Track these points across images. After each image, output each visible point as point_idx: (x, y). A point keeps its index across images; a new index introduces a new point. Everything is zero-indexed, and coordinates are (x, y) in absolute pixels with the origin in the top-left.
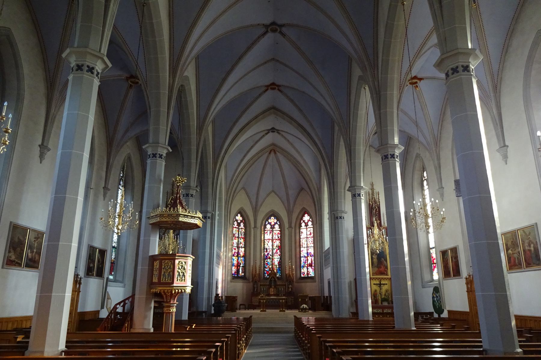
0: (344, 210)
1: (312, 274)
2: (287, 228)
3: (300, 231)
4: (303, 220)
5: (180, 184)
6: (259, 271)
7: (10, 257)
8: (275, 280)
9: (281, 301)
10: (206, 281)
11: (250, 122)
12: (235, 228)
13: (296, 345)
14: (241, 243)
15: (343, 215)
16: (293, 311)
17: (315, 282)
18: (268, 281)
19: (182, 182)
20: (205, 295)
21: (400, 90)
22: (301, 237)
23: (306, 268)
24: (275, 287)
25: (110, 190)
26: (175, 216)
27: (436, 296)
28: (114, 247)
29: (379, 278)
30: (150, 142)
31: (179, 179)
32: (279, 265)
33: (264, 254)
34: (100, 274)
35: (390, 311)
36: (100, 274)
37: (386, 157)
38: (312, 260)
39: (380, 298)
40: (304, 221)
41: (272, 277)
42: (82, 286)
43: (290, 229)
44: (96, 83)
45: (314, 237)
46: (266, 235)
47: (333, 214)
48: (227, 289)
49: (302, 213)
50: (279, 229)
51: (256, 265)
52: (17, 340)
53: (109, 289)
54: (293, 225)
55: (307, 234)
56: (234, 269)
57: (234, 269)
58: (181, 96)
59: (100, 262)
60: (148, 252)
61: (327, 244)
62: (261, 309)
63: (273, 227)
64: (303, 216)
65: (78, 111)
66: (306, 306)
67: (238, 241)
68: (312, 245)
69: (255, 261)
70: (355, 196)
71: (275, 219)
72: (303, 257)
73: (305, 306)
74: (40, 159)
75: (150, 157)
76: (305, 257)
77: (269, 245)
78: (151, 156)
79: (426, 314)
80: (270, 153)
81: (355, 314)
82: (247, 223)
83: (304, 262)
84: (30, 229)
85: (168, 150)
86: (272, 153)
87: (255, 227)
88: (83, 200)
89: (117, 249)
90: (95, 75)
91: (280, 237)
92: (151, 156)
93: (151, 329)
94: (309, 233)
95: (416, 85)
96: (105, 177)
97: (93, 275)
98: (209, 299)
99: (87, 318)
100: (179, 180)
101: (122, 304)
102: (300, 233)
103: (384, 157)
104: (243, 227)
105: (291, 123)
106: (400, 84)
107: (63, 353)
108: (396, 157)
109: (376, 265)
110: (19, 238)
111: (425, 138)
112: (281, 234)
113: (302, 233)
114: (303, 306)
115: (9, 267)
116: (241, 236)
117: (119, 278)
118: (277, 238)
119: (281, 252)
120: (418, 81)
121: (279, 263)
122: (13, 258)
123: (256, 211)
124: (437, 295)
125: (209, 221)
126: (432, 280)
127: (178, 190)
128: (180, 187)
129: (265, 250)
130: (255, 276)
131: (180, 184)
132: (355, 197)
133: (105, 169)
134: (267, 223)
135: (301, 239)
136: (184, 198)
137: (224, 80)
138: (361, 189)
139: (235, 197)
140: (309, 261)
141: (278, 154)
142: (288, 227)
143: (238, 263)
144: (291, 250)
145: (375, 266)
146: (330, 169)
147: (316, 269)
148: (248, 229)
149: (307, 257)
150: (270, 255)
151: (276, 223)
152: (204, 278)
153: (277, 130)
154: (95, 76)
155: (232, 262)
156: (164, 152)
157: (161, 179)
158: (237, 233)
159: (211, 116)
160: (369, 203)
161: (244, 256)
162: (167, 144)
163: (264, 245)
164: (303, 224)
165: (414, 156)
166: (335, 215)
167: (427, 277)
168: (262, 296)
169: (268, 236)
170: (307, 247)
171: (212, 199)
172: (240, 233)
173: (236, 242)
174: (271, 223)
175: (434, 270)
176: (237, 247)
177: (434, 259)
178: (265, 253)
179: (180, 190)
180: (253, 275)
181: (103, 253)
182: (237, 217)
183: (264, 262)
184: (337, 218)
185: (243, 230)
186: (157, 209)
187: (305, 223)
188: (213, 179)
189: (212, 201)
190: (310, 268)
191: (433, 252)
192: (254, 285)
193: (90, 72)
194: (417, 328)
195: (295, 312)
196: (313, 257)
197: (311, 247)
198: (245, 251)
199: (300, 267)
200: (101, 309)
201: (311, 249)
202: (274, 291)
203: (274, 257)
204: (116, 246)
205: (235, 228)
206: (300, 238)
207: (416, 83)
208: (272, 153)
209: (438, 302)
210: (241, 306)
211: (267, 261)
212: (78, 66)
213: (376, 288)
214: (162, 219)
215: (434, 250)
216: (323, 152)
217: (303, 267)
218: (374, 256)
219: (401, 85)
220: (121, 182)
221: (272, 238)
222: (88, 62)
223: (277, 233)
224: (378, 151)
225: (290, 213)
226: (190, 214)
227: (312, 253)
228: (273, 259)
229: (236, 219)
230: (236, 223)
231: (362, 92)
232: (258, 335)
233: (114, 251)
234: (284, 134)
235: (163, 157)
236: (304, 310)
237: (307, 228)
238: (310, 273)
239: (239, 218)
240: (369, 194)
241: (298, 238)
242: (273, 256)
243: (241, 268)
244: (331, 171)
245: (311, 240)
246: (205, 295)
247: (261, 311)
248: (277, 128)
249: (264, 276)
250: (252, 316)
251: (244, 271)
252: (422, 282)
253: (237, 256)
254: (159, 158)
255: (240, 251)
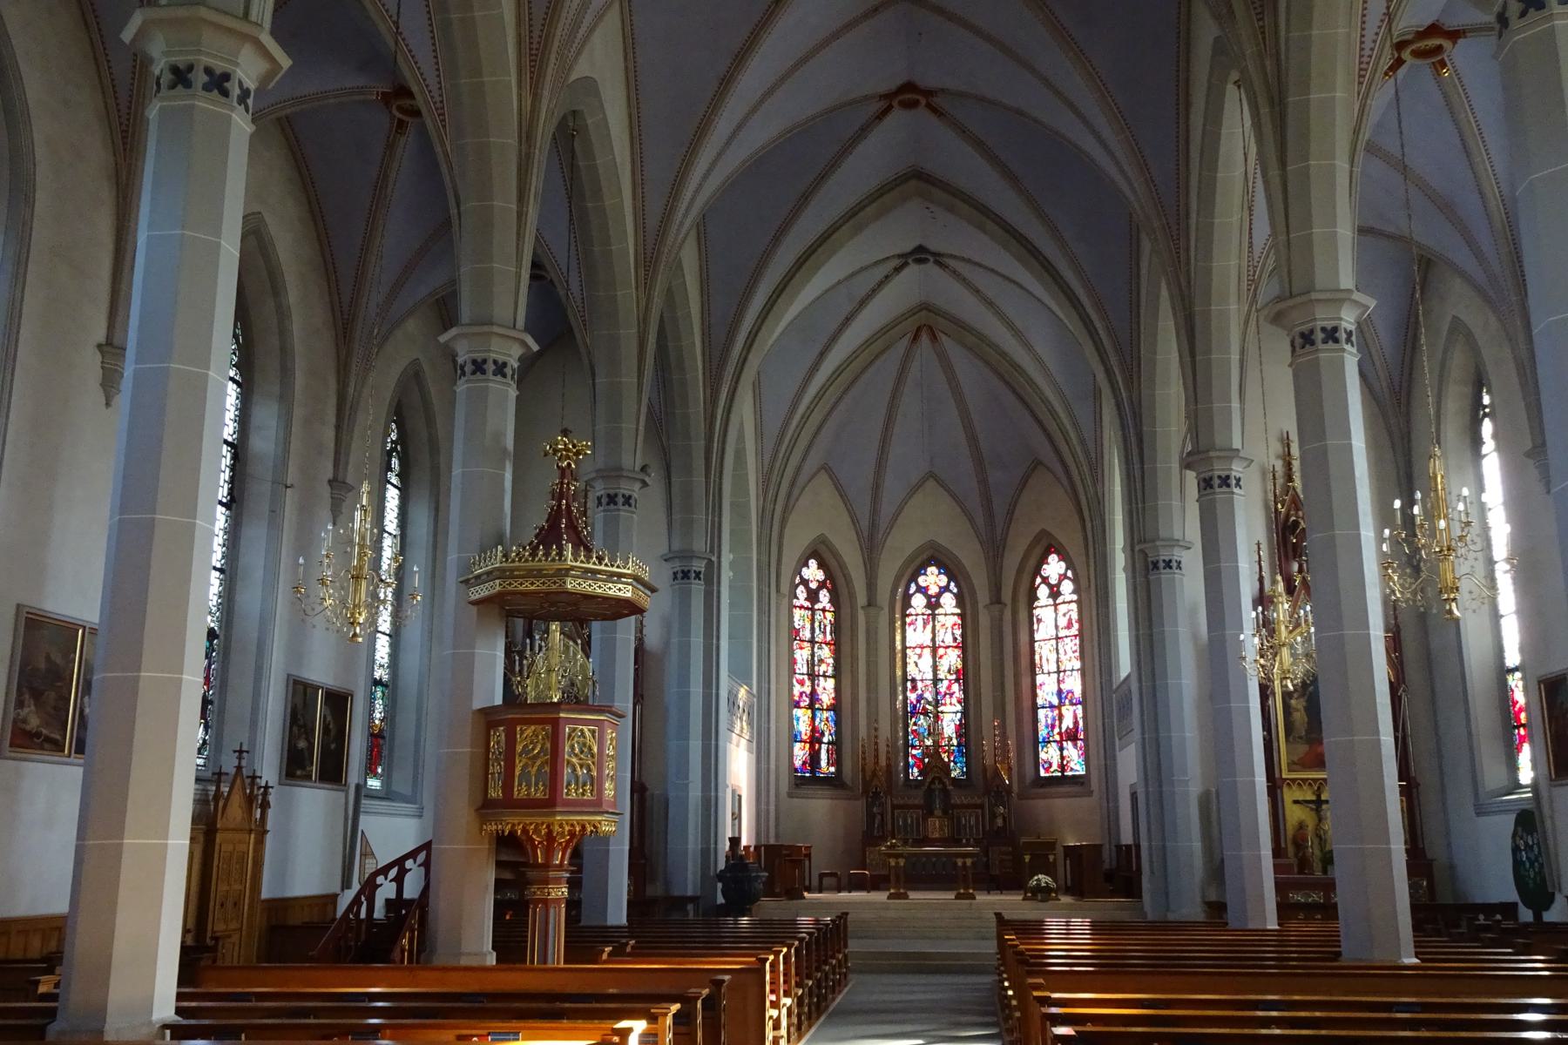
0: (1181, 538)
1: (1077, 766)
2: (986, 607)
3: (1031, 616)
4: (1042, 577)
5: (569, 464)
6: (888, 758)
7: (25, 721)
8: (945, 791)
9: (892, 862)
10: (695, 792)
11: (834, 232)
12: (801, 607)
13: (993, 1014)
14: (821, 661)
15: (1177, 554)
16: (1008, 898)
17: (1090, 793)
18: (921, 793)
19: (577, 453)
20: (693, 843)
21: (1360, 83)
22: (1037, 637)
23: (1054, 744)
24: (945, 812)
25: (353, 488)
26: (552, 576)
27: (1526, 844)
28: (378, 683)
29: (1315, 780)
30: (463, 322)
31: (565, 444)
32: (959, 736)
33: (905, 698)
34: (333, 773)
35: (1316, 897)
36: (333, 773)
37: (1307, 338)
38: (1075, 717)
39: (1317, 852)
40: (1047, 578)
41: (933, 779)
42: (271, 813)
43: (997, 607)
44: (241, 124)
45: (1081, 635)
46: (909, 630)
47: (1142, 551)
48: (777, 818)
49: (1038, 551)
50: (958, 611)
51: (876, 737)
52: (37, 989)
53: (365, 822)
54: (1007, 595)
55: (1057, 627)
56: (802, 753)
57: (800, 753)
58: (573, 151)
59: (333, 733)
60: (469, 697)
61: (1125, 665)
62: (889, 890)
63: (933, 604)
64: (1043, 560)
65: (183, 228)
66: (1049, 879)
67: (813, 655)
68: (1078, 665)
69: (873, 719)
70: (1214, 485)
71: (940, 573)
72: (1043, 707)
73: (1044, 879)
74: (105, 390)
75: (463, 374)
76: (1052, 707)
77: (920, 667)
78: (469, 368)
79: (1490, 909)
80: (916, 337)
81: (1217, 909)
82: (843, 591)
83: (1047, 726)
84: (84, 628)
85: (524, 344)
86: (925, 338)
87: (871, 603)
88: (1364, 446)
89: (390, 687)
90: (235, 99)
91: (959, 639)
92: (466, 369)
93: (489, 958)
94: (1063, 622)
95: (1439, 58)
96: (332, 445)
97: (308, 777)
98: (707, 853)
99: (296, 918)
100: (564, 450)
101: (393, 873)
102: (1031, 624)
103: (1299, 341)
104: (828, 606)
105: (981, 228)
106: (1361, 63)
107: (168, 1032)
108: (1344, 336)
109: (1304, 733)
110: (48, 658)
111: (1478, 254)
112: (963, 626)
113: (1039, 621)
114: (1038, 880)
115: (19, 755)
116: (821, 636)
117: (401, 784)
118: (949, 640)
119: (965, 691)
120: (1446, 44)
121: (958, 728)
122: (34, 722)
123: (871, 547)
124: (1531, 843)
125: (698, 588)
126: (1516, 786)
127: (562, 483)
128: (568, 472)
129: (909, 685)
130: (874, 774)
131: (569, 464)
132: (1211, 487)
133: (331, 418)
134: (913, 588)
135: (1036, 644)
136: (601, 508)
137: (726, 82)
138: (1230, 459)
139: (797, 500)
140: (1068, 723)
141: (944, 338)
142: (988, 601)
143: (814, 729)
144: (1003, 684)
145: (1301, 738)
146: (1129, 389)
147: (1093, 751)
148: (846, 611)
149: (1059, 707)
150: (929, 703)
151: (946, 589)
152: (687, 785)
153: (934, 254)
154: (235, 104)
155: (791, 726)
156: (512, 355)
157: (506, 449)
158: (808, 626)
159: (685, 216)
160: (1276, 509)
161: (835, 707)
162: (521, 322)
163: (905, 664)
164: (1043, 592)
165: (1445, 328)
166: (1146, 555)
167: (1493, 775)
168: (893, 846)
169: (917, 635)
170: (1058, 672)
171: (707, 509)
172: (817, 624)
173: (805, 658)
174: (927, 588)
175: (1519, 750)
176: (808, 674)
177: (1521, 710)
178: (908, 694)
179: (568, 484)
180: (869, 773)
181: (338, 701)
182: (804, 570)
183: (906, 725)
184: (1155, 565)
185: (829, 616)
186: (491, 552)
187: (1051, 587)
188: (709, 439)
189: (707, 515)
190: (1068, 745)
191: (1515, 682)
192: (869, 807)
193: (216, 91)
194: (1423, 960)
195: (1011, 903)
196: (1080, 707)
197: (1073, 670)
198: (837, 689)
199: (1036, 742)
200: (343, 890)
201: (1072, 678)
202: (941, 829)
203: (939, 709)
204: (385, 678)
205: (801, 607)
206: (1032, 641)
207: (1439, 49)
208: (925, 338)
209: (1532, 865)
210: (826, 881)
211: (915, 724)
212: (175, 70)
213: (1303, 817)
214: (510, 584)
215: (1518, 675)
216: (1098, 324)
217: (1044, 741)
218: (1293, 702)
219: (1363, 66)
220: (395, 462)
221: (933, 640)
222: (494, 352)
223: (949, 625)
224: (1277, 319)
225: (994, 550)
226: (603, 567)
227: (1078, 693)
228: (937, 717)
229: (801, 577)
230: (801, 592)
231: (1226, 123)
232: (868, 978)
233: (379, 694)
234: (952, 263)
235: (508, 371)
236: (1042, 893)
237: (1056, 605)
238: (1072, 765)
239: (813, 573)
240: (1274, 475)
241: (1024, 638)
242: (937, 703)
243: (824, 747)
244: (1130, 398)
245: (1071, 646)
246: (693, 843)
247: (957, 897)
248: (933, 246)
249: (907, 774)
250: (847, 914)
251: (837, 761)
252: (1476, 794)
253: (811, 706)
254: (495, 374)
255: (819, 690)
